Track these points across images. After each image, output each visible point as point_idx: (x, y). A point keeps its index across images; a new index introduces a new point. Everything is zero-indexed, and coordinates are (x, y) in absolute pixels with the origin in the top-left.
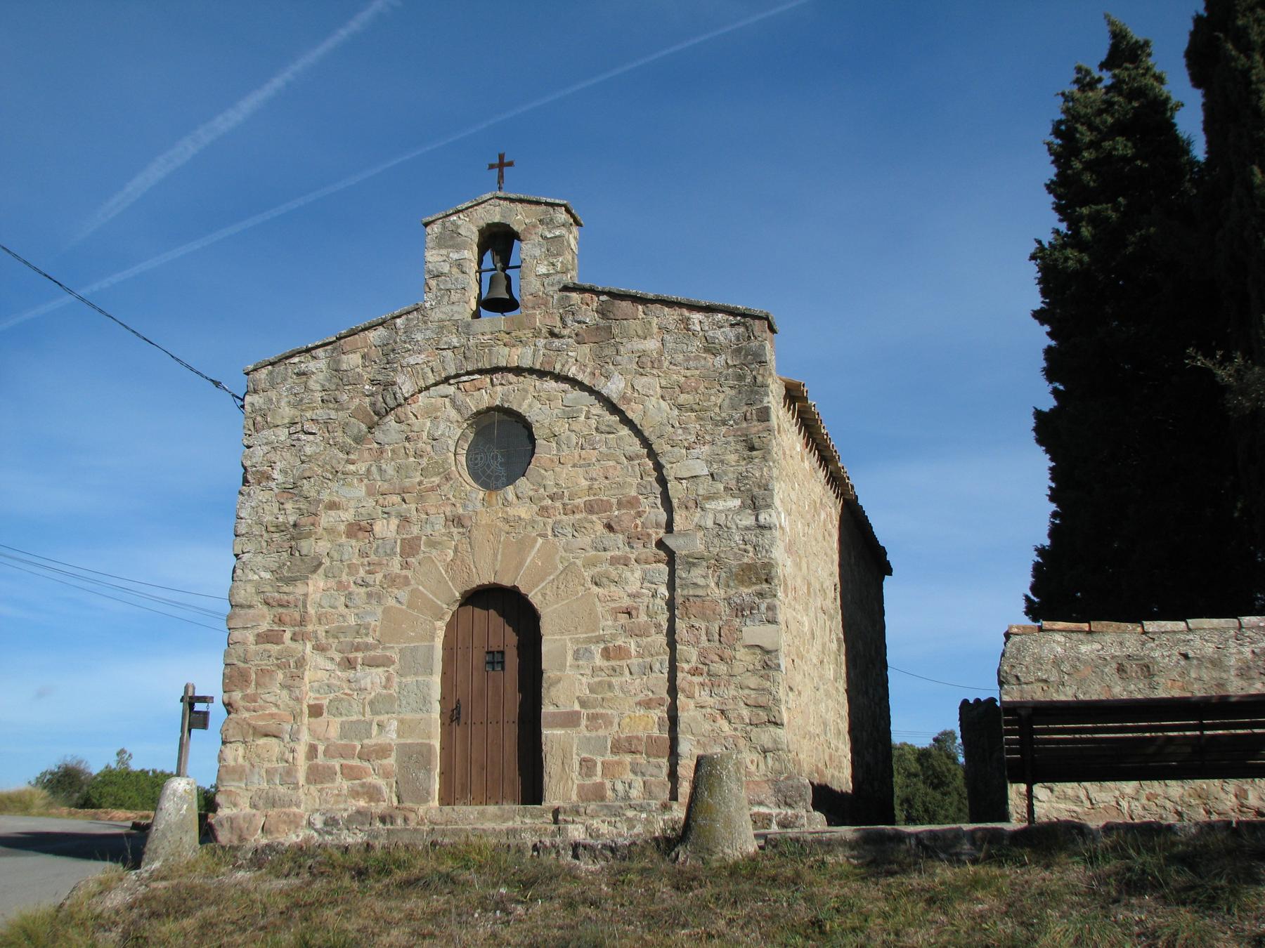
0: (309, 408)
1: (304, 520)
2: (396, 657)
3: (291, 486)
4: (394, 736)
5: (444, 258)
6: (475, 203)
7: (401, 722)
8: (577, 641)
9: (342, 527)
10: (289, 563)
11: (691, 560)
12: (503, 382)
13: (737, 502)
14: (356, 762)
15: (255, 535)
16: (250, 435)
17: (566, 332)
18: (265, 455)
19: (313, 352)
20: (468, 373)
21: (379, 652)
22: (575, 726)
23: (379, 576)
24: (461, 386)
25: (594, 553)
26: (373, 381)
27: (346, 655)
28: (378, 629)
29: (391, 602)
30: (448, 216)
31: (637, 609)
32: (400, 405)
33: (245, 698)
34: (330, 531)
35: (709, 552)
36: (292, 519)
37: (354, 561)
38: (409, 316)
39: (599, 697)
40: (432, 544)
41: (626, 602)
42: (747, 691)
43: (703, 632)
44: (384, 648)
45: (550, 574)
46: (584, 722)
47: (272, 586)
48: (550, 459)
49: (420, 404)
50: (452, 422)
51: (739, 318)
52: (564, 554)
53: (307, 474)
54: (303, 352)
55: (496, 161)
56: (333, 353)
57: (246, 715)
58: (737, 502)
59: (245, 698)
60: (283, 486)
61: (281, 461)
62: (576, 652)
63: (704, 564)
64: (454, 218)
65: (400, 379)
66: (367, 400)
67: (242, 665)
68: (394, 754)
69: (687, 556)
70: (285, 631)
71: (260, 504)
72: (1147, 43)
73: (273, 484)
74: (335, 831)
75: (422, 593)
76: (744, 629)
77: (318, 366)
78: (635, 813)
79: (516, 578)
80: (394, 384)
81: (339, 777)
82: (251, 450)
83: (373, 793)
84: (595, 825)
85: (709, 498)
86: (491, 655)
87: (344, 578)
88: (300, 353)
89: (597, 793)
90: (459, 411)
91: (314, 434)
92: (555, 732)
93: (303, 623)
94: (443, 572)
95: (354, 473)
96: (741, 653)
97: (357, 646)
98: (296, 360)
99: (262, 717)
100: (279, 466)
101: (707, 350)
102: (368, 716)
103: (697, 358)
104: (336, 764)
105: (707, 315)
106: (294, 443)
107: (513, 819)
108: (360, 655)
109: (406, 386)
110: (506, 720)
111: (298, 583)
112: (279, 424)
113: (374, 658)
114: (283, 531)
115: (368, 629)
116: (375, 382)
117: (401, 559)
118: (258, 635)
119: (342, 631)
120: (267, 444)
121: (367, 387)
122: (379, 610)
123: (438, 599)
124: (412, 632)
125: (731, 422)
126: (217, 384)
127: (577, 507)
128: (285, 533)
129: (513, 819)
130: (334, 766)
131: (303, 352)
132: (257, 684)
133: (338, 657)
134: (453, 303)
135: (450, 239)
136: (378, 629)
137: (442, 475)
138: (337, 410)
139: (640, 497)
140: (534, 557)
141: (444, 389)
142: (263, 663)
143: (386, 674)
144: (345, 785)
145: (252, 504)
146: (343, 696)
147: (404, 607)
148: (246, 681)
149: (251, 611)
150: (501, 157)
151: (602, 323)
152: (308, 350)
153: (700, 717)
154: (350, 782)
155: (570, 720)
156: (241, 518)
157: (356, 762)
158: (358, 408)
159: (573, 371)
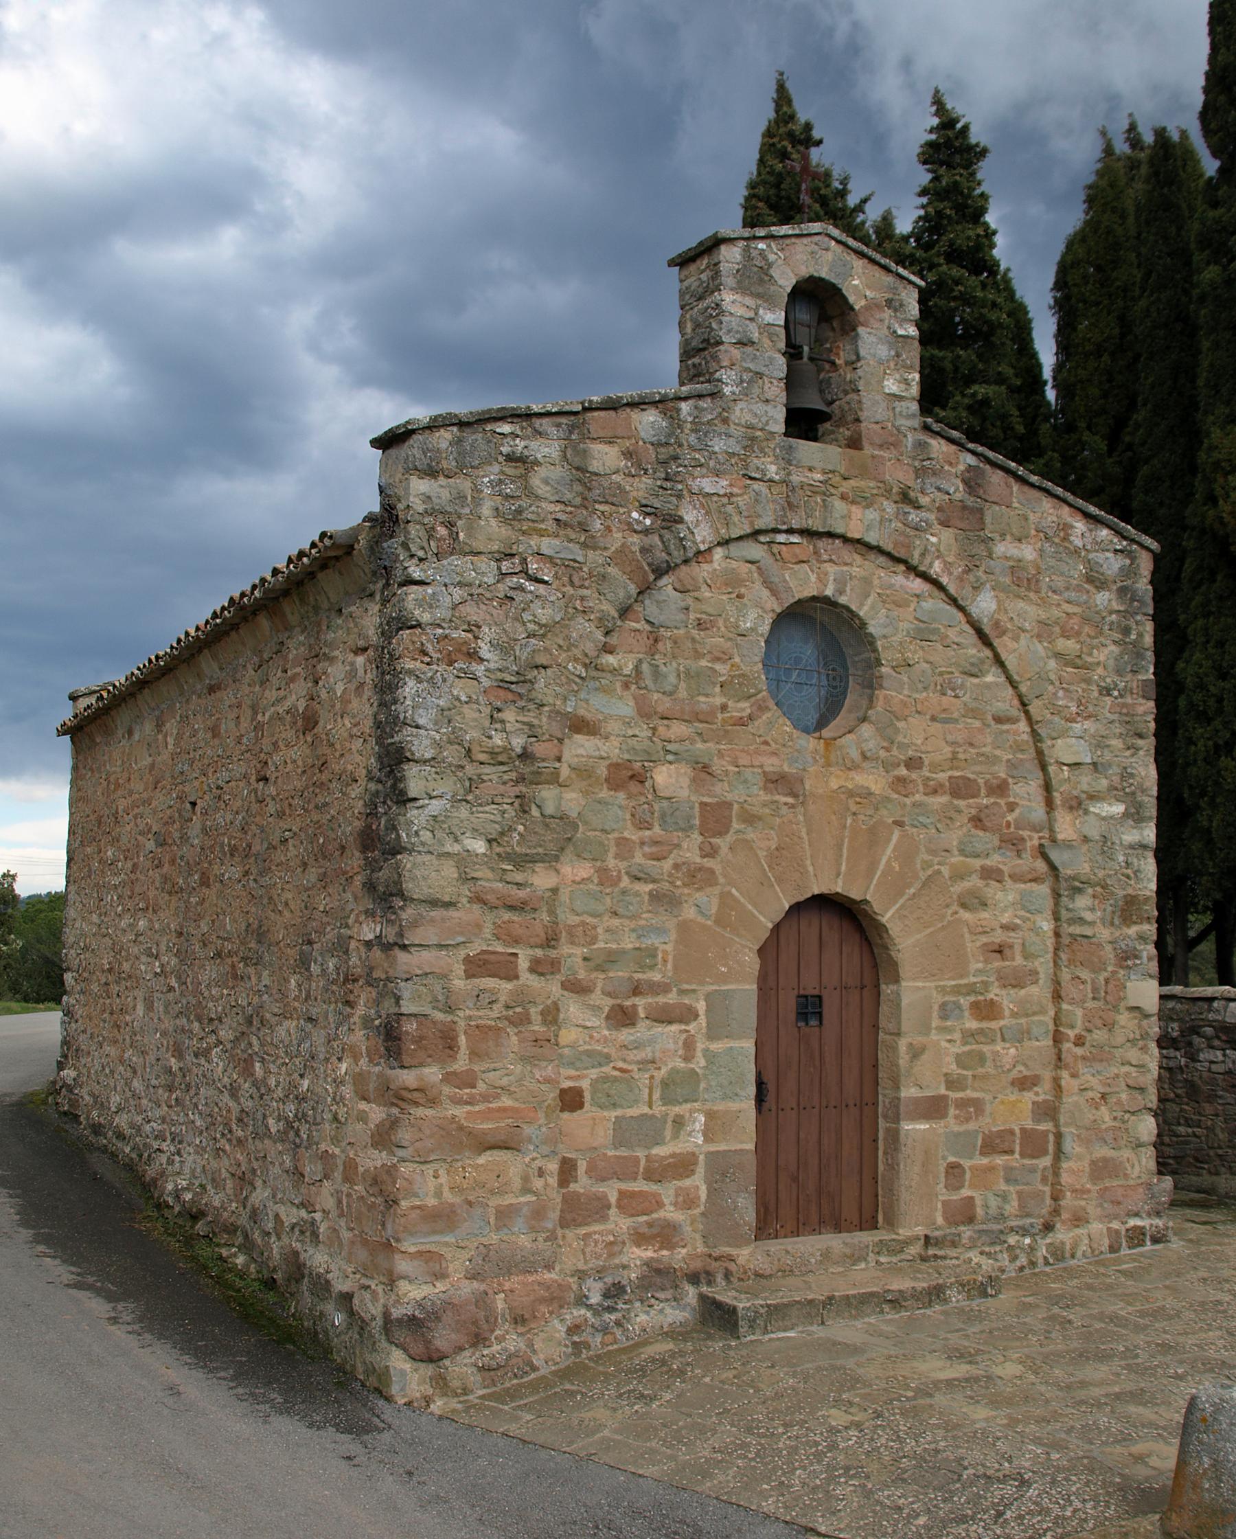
0: (535, 529)
1: (539, 749)
2: (701, 1006)
3: (513, 679)
4: (700, 1141)
5: (751, 315)
7: (710, 1115)
8: (942, 990)
9: (602, 771)
10: (521, 828)
11: (1077, 884)
14: (640, 1186)
15: (450, 765)
16: (421, 560)
17: (924, 500)
18: (455, 607)
19: (537, 422)
20: (790, 531)
21: (672, 998)
23: (667, 865)
24: (775, 548)
25: (962, 858)
26: (646, 506)
27: (619, 1001)
28: (670, 958)
29: (689, 913)
30: (755, 238)
31: (1011, 947)
32: (686, 562)
33: (448, 1078)
34: (583, 772)
35: (1095, 874)
36: (518, 742)
37: (626, 834)
38: (701, 403)
39: (970, 1073)
40: (750, 819)
41: (999, 937)
42: (1127, 1068)
43: (1089, 987)
44: (682, 992)
45: (909, 886)
46: (952, 1111)
47: (492, 869)
48: (902, 701)
49: (716, 565)
50: (765, 612)
51: (1125, 543)
52: (927, 857)
53: (542, 659)
54: (519, 416)
56: (571, 433)
57: (459, 1112)
58: (1119, 808)
59: (448, 1078)
60: (500, 675)
61: (489, 626)
62: (943, 1006)
63: (1090, 891)
64: (761, 245)
65: (690, 514)
66: (635, 539)
67: (439, 1016)
68: (701, 1170)
69: (1074, 879)
70: (515, 955)
71: (457, 703)
72: (984, 152)
73: (479, 669)
74: (621, 1306)
75: (737, 901)
76: (1128, 984)
78: (1017, 1238)
79: (868, 888)
80: (680, 520)
81: (613, 1211)
83: (666, 1235)
84: (975, 1260)
85: (1093, 797)
87: (611, 862)
89: (964, 1214)
90: (774, 593)
91: (545, 582)
92: (918, 1127)
93: (553, 943)
94: (766, 866)
95: (615, 671)
96: (1124, 1018)
97: (637, 987)
98: (506, 428)
99: (487, 1115)
100: (487, 632)
101: (1090, 580)
102: (658, 1109)
103: (1079, 588)
104: (612, 1191)
105: (1092, 526)
106: (511, 593)
107: (865, 1260)
108: (640, 1002)
110: (824, 1104)
111: (539, 867)
112: (482, 549)
113: (665, 1008)
114: (502, 763)
115: (654, 956)
116: (648, 510)
117: (700, 838)
118: (467, 960)
119: (612, 958)
120: (460, 584)
121: (635, 515)
122: (671, 924)
123: (761, 913)
124: (724, 965)
127: (942, 785)
128: (505, 768)
129: (865, 1260)
130: (605, 1196)
131: (519, 416)
132: (474, 1054)
133: (607, 1003)
134: (767, 401)
136: (670, 958)
137: (753, 699)
138: (584, 546)
139: (1010, 780)
140: (890, 857)
141: (755, 550)
142: (481, 1013)
143: (684, 1036)
144: (620, 1223)
145: (441, 703)
146: (617, 1073)
147: (709, 923)
148: (450, 1048)
149: (452, 913)
151: (970, 500)
152: (529, 416)
153: (1082, 1101)
154: (632, 1219)
155: (933, 1108)
156: (417, 727)
157: (640, 1186)
158: (623, 550)
159: (936, 568)
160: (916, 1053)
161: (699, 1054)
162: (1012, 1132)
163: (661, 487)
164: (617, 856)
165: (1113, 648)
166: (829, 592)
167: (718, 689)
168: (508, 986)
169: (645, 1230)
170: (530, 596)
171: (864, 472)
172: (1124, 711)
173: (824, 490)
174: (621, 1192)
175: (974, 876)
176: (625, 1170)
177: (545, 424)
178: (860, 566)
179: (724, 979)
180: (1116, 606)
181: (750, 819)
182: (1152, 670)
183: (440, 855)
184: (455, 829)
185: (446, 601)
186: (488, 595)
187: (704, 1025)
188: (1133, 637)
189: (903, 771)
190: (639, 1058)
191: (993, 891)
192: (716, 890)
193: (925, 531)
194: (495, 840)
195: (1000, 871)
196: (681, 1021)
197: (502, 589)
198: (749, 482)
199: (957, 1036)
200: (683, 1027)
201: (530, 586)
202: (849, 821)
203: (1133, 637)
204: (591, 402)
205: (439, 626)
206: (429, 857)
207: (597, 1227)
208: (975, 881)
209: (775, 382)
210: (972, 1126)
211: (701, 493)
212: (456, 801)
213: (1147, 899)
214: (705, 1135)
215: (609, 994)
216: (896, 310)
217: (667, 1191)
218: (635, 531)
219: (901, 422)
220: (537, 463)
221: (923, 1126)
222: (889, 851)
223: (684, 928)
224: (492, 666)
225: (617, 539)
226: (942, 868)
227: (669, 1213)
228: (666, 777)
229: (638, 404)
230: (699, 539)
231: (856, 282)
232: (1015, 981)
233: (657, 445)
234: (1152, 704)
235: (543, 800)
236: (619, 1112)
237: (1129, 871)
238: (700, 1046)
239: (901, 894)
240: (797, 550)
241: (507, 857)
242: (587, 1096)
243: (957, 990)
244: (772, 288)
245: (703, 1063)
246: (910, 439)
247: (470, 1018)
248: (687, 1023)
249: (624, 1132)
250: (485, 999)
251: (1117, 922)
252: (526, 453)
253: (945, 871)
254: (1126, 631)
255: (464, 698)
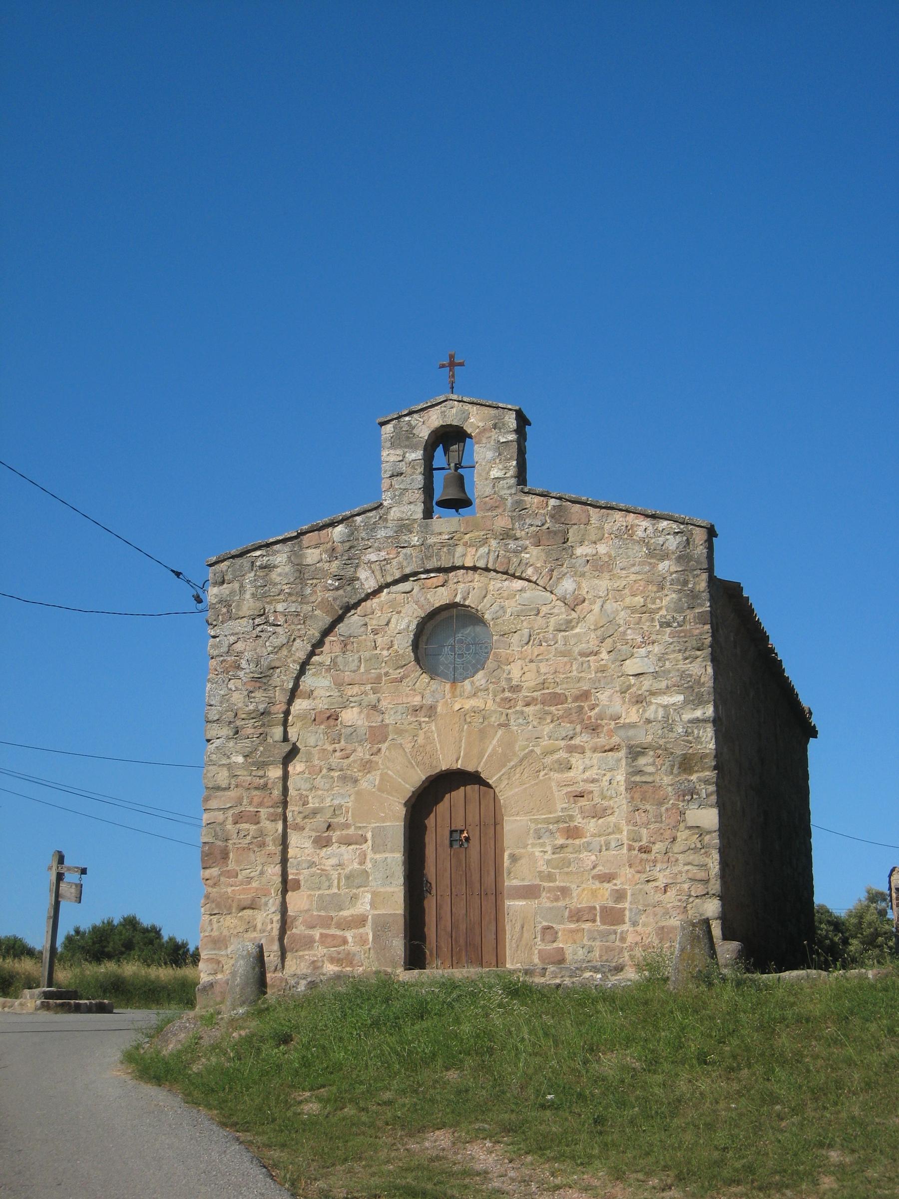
2: (369, 835)
3: (259, 676)
4: (368, 908)
5: (401, 458)
6: (429, 404)
7: (375, 894)
12: (314, 777)
13: (681, 698)
21: (351, 831)
22: (536, 898)
26: (336, 576)
41: (579, 788)
51: (682, 527)
55: (457, 360)
60: (252, 675)
62: (537, 831)
64: (407, 419)
73: (241, 674)
77: (281, 557)
79: (479, 763)
82: (218, 639)
85: (653, 694)
86: (454, 843)
88: (259, 548)
91: (280, 625)
98: (258, 553)
102: (344, 891)
109: (367, 580)
119: (315, 812)
120: (233, 634)
121: (330, 582)
125: (675, 624)
126: (178, 574)
128: (254, 720)
135: (404, 439)
144: (320, 951)
150: (452, 357)
152: (268, 545)
155: (530, 892)
157: (333, 931)
160: (514, 858)
161: (368, 860)
162: (594, 908)
163: (345, 564)
164: (631, 903)
165: (674, 595)
166: (457, 600)
167: (383, 664)
168: (253, 827)
169: (335, 955)
170: (270, 634)
171: (476, 527)
172: (682, 634)
173: (452, 543)
174: (321, 934)
175: (561, 751)
176: (326, 922)
177: (277, 547)
178: (478, 580)
179: (383, 820)
180: (673, 569)
181: (400, 732)
182: (708, 604)
183: (220, 766)
184: (227, 752)
185: (226, 644)
186: (248, 637)
187: (370, 845)
188: (690, 586)
189: (507, 694)
190: (331, 863)
191: (576, 760)
192: (379, 772)
193: (521, 552)
194: (248, 756)
195: (583, 748)
196: (356, 844)
197: (255, 633)
198: (400, 550)
199: (549, 849)
200: (358, 847)
201: (270, 629)
202: (466, 727)
203: (690, 586)
204: (301, 529)
205: (222, 656)
206: (214, 767)
207: (307, 953)
208: (562, 754)
209: (416, 491)
210: (561, 904)
211: (370, 562)
212: (228, 738)
213: (704, 756)
214: (371, 905)
215: (313, 830)
216: (500, 429)
217: (349, 935)
218: (329, 590)
219: (502, 493)
220: (275, 567)
221: (522, 903)
222: (494, 742)
223: (359, 793)
224: (248, 671)
225: (320, 595)
226: (535, 749)
227: (352, 947)
228: (350, 716)
229: (332, 524)
230: (367, 587)
231: (472, 420)
232: (598, 813)
233: (343, 542)
234: (708, 627)
235: (273, 734)
236: (320, 892)
237: (690, 738)
238: (368, 857)
239: (505, 766)
240: (435, 580)
241: (253, 764)
242: (302, 883)
243: (547, 821)
244: (415, 440)
245: (370, 865)
246: (510, 501)
247: (235, 844)
248: (361, 844)
249: (324, 903)
250: (242, 834)
251: (675, 771)
252: (269, 563)
253: (538, 750)
254: (686, 583)
255: (234, 689)
